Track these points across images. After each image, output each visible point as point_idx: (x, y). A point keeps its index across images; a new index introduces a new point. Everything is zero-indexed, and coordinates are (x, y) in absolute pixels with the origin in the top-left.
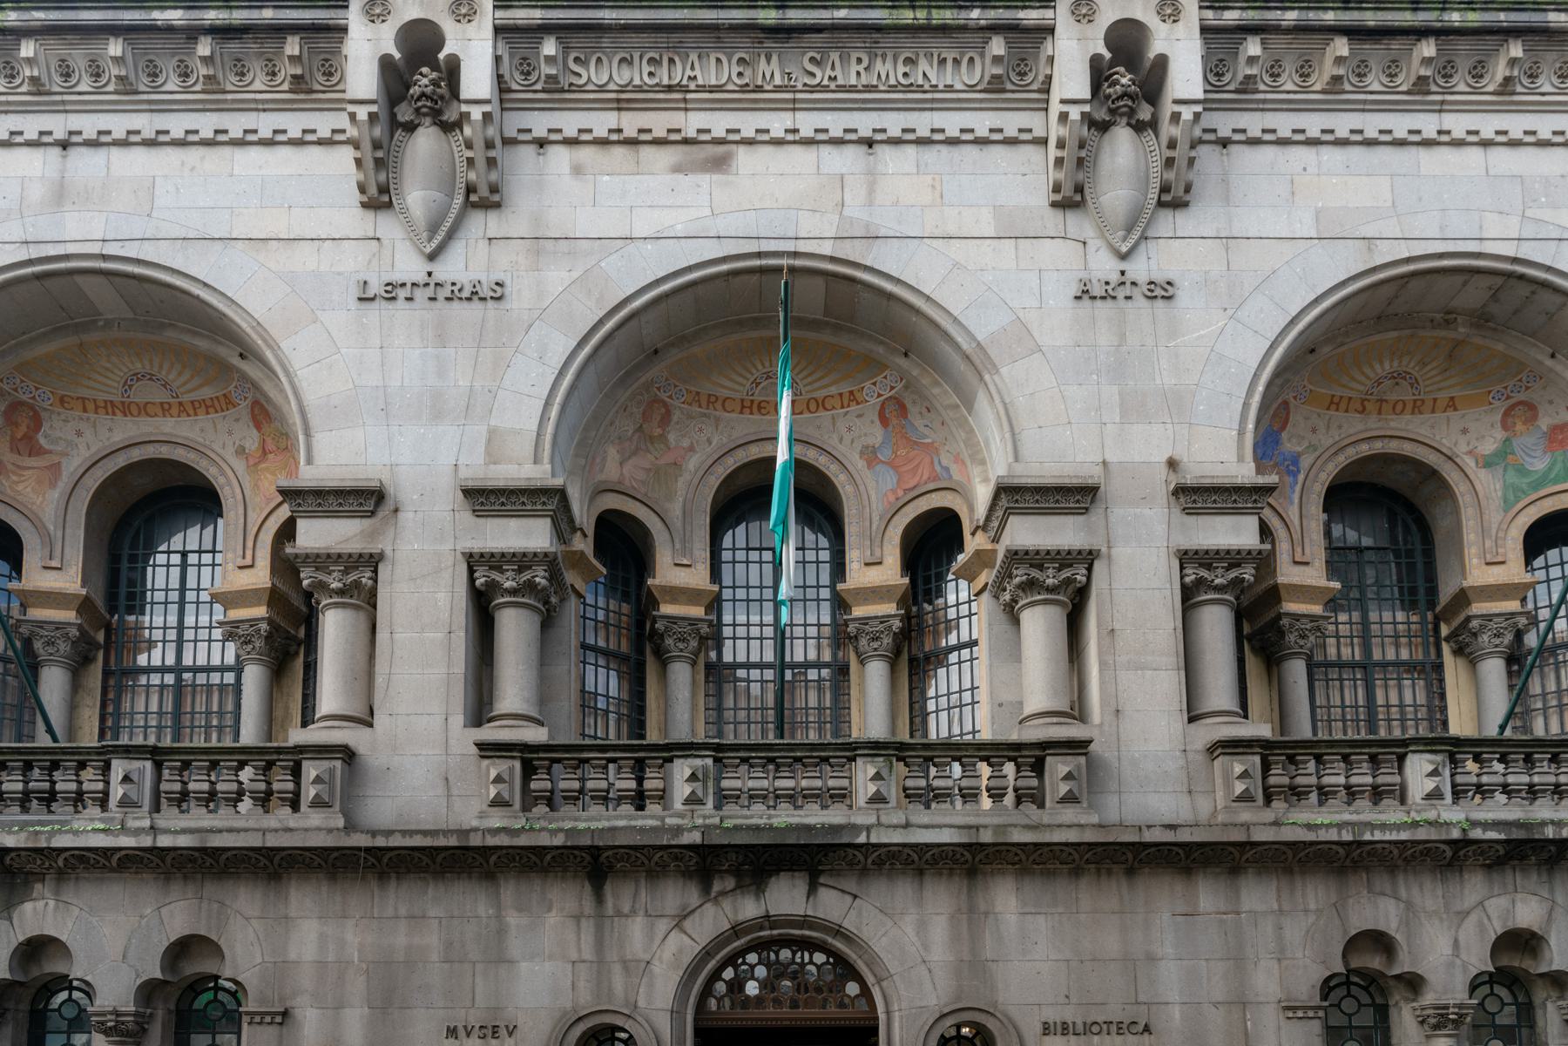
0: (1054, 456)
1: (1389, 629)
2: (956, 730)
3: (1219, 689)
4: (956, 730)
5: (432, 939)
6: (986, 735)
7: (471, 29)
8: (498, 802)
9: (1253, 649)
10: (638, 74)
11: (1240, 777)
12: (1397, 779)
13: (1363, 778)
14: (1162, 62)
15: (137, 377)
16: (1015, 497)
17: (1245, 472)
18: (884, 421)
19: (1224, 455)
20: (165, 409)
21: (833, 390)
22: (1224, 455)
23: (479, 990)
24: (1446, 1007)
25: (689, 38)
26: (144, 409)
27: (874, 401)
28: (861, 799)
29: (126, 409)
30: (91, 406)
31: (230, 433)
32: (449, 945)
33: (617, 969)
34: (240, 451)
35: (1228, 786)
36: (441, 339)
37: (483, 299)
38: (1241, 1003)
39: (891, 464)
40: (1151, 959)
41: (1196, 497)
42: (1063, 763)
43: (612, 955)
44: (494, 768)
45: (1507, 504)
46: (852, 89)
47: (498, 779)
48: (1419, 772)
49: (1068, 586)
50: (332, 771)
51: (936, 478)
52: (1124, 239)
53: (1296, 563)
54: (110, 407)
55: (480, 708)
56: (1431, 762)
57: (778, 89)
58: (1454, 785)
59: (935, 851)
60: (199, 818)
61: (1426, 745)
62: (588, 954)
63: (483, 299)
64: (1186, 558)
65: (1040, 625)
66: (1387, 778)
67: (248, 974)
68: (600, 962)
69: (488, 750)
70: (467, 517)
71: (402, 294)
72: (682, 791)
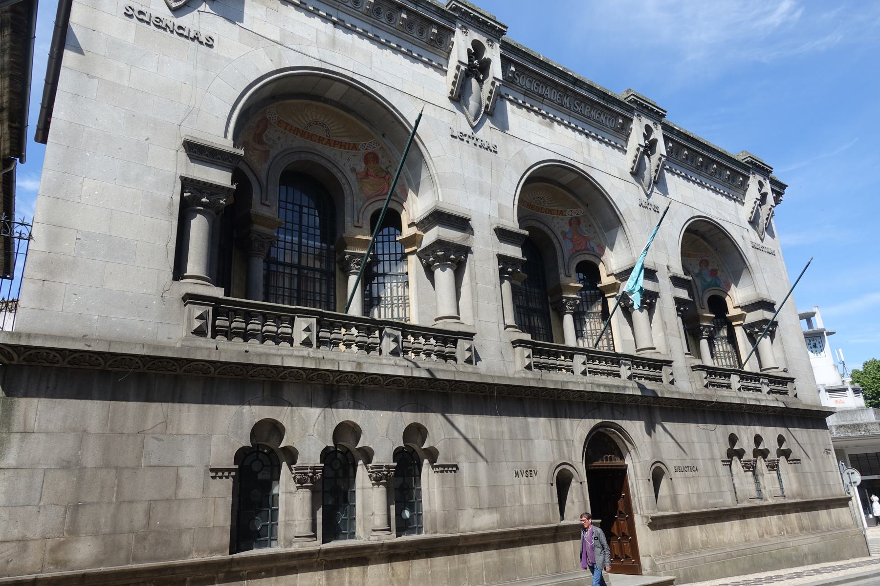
0: (456, 203)
1: (288, 246)
2: (396, 316)
3: (195, 264)
4: (396, 316)
5: (505, 428)
6: (414, 321)
7: (493, 50)
8: (200, 332)
9: (553, 310)
10: (534, 87)
11: (198, 318)
12: (290, 331)
13: (270, 327)
14: (488, 62)
15: (317, 123)
16: (438, 217)
17: (226, 144)
18: (570, 224)
19: (218, 134)
20: (320, 140)
21: (556, 208)
22: (218, 134)
23: (523, 452)
24: (306, 468)
25: (549, 83)
26: (311, 137)
27: (363, 152)
28: (297, 343)
29: (303, 134)
30: (288, 128)
31: (349, 160)
32: (511, 431)
33: (564, 443)
34: (353, 170)
35: (702, 382)
36: (479, 161)
37: (201, 43)
38: (713, 459)
39: (571, 240)
40: (693, 443)
41: (503, 234)
42: (199, 309)
43: (562, 438)
44: (198, 310)
45: (703, 291)
46: (584, 115)
47: (200, 317)
48: (735, 379)
49: (454, 257)
50: (207, 312)
51: (588, 250)
52: (474, 121)
53: (262, 204)
54: (296, 131)
55: (179, 272)
56: (306, 322)
57: (567, 108)
58: (318, 337)
59: (33, 351)
60: (238, 344)
61: (736, 372)
62: (555, 438)
63: (201, 43)
64: (187, 183)
65: (444, 276)
66: (285, 329)
67: (439, 444)
68: (559, 440)
69: (190, 299)
70: (183, 155)
71: (466, 139)
72: (300, 335)
